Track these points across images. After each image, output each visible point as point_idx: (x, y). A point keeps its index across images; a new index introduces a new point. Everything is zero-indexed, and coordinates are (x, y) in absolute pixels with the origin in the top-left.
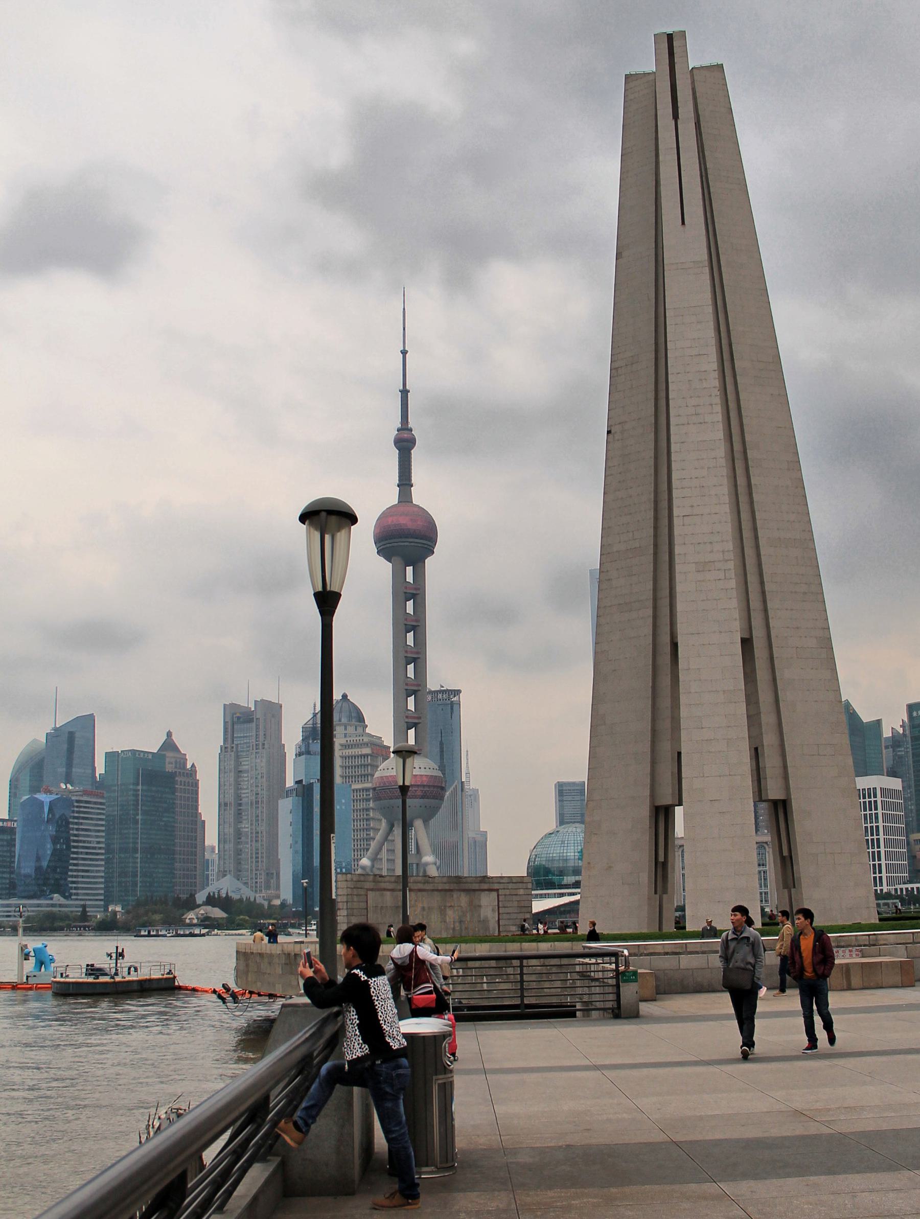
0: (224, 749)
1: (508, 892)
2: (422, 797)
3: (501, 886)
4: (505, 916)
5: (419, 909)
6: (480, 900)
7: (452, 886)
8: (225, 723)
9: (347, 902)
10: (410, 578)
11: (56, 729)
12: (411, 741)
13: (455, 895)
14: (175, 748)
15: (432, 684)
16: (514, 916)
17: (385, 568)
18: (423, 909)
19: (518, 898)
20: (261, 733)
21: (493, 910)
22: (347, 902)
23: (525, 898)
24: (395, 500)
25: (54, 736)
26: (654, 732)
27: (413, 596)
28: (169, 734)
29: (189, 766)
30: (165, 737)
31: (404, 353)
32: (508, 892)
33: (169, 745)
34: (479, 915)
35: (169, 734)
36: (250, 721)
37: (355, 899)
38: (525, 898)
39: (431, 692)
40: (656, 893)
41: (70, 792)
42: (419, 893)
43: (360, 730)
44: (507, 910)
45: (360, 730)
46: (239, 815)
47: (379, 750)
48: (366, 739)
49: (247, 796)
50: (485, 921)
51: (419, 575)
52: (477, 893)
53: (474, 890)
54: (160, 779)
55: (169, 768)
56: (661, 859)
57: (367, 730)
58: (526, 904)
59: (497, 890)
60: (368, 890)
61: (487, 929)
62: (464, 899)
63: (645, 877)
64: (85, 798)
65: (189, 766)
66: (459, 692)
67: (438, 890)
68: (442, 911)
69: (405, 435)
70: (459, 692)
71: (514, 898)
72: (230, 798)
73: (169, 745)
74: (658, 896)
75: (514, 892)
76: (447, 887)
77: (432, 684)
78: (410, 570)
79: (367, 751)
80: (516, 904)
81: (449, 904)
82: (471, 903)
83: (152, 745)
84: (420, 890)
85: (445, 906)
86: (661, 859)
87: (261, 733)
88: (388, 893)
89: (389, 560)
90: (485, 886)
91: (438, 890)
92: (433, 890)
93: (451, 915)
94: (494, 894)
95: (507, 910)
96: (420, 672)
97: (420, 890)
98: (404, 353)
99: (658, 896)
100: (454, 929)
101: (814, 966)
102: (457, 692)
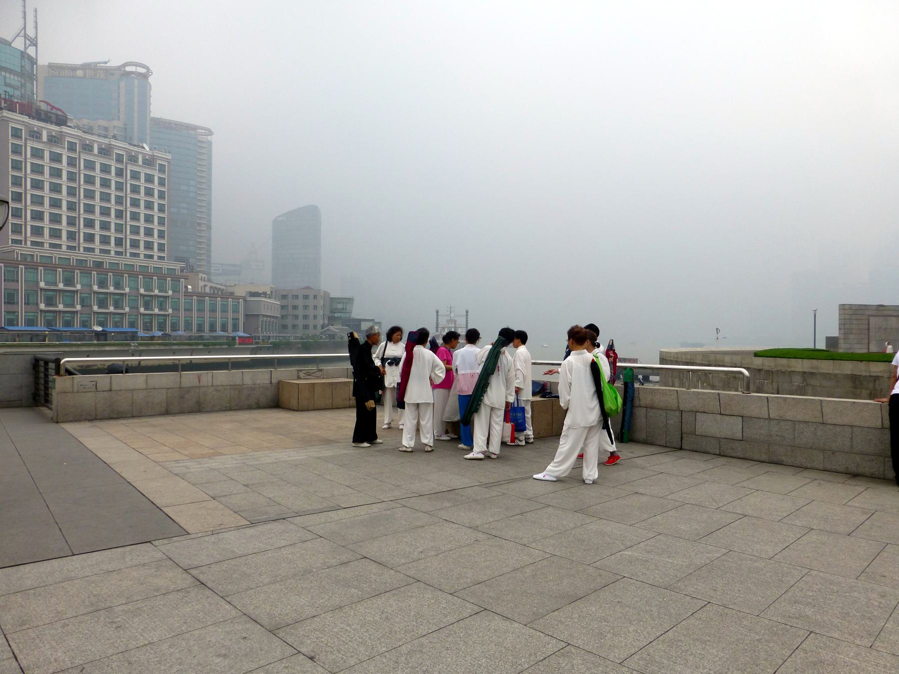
37: (855, 322)
60: (869, 316)
88: (894, 319)
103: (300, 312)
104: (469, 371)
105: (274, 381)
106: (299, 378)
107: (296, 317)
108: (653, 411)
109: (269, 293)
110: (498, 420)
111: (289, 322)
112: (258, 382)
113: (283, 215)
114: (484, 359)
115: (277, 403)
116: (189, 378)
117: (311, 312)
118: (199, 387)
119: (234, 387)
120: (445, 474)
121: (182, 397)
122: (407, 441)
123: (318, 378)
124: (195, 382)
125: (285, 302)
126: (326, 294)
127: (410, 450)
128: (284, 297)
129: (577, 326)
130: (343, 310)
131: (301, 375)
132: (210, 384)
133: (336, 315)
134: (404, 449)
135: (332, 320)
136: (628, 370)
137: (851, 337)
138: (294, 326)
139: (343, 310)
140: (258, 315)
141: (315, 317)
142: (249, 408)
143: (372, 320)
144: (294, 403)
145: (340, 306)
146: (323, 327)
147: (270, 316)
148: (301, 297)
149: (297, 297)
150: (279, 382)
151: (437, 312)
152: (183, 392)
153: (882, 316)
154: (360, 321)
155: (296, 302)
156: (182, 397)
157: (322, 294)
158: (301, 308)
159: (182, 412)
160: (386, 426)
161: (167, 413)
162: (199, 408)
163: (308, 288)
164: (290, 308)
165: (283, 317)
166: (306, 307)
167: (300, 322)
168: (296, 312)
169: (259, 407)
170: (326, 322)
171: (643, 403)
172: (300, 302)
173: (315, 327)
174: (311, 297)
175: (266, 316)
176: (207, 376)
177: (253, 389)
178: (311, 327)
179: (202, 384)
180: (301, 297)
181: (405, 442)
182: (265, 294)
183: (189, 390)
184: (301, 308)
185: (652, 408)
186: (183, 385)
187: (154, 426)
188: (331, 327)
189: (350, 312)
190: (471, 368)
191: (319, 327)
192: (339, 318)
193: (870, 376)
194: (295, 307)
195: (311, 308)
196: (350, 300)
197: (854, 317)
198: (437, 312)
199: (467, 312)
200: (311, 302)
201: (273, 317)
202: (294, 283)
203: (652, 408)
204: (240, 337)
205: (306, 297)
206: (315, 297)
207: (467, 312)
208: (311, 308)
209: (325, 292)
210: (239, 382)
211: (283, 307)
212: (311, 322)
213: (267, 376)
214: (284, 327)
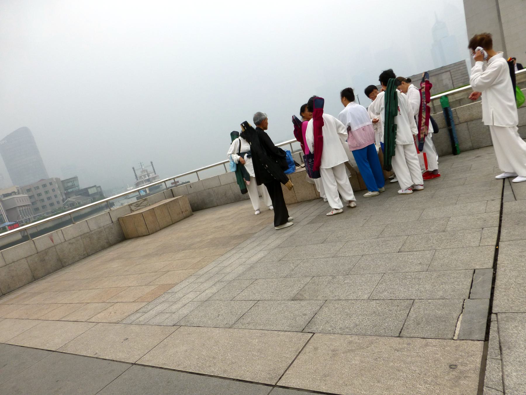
1: (455, 70)
19: (460, 71)
32: (455, 70)
59: (449, 71)
94: (448, 73)
103: (44, 196)
104: (360, 126)
105: (114, 220)
106: (132, 211)
107: (43, 200)
108: (474, 122)
109: (16, 191)
110: (413, 155)
111: (39, 205)
112: (102, 225)
113: (4, 139)
114: (383, 106)
115: (123, 237)
116: (42, 242)
117: (51, 194)
118: (55, 246)
119: (83, 236)
120: (384, 217)
121: (43, 260)
122: (336, 204)
123: (146, 206)
124: (50, 244)
125: (31, 194)
126: (57, 180)
127: (341, 211)
128: (29, 190)
129: (379, 80)
130: (73, 186)
131: (133, 208)
132: (63, 241)
133: (69, 191)
134: (335, 212)
135: (68, 195)
136: (444, 98)
138: (44, 207)
139: (73, 186)
140: (15, 208)
141: (56, 196)
142: (104, 248)
143: (95, 186)
144: (142, 229)
145: (70, 184)
146: (63, 201)
147: (24, 206)
148: (41, 187)
149: (38, 188)
150: (118, 219)
151: (133, 168)
152: (42, 255)
154: (86, 189)
155: (39, 191)
156: (43, 260)
157: (55, 180)
158: (43, 194)
159: (48, 273)
160: (256, 213)
161: (35, 279)
162: (61, 264)
163: (42, 180)
164: (36, 196)
165: (33, 203)
166: (47, 192)
167: (47, 203)
168: (41, 198)
169: (110, 245)
170: (64, 197)
171: (461, 120)
172: (42, 190)
173: (58, 202)
174: (48, 185)
175: (21, 206)
176: (57, 235)
177: (101, 232)
178: (55, 203)
179: (55, 244)
180: (41, 187)
181: (334, 205)
182: (14, 193)
183: (46, 252)
184: (43, 194)
185: (472, 120)
186: (39, 249)
187: (39, 293)
188: (69, 199)
189: (78, 186)
190: (362, 122)
191: (61, 202)
192: (72, 192)
193: (456, 101)
194: (39, 195)
195: (51, 191)
196: (75, 179)
198: (133, 168)
199: (152, 163)
200: (49, 188)
201: (26, 205)
202: (31, 180)
203: (472, 120)
204: (8, 226)
205: (44, 186)
206: (51, 184)
207: (152, 163)
208: (51, 191)
209: (56, 179)
210: (86, 230)
211: (30, 197)
212: (54, 200)
213: (108, 217)
214: (37, 209)
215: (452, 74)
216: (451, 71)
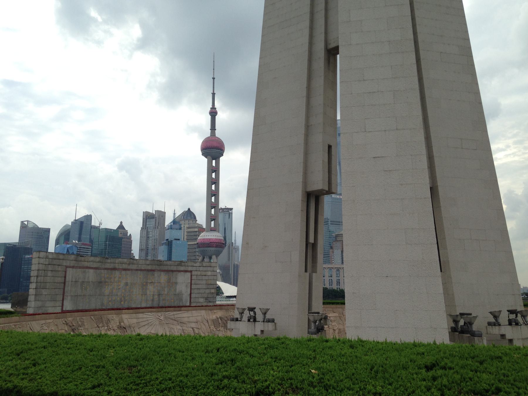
0: (142, 228)
1: (199, 273)
2: (216, 247)
3: (194, 269)
4: (196, 291)
5: (122, 284)
6: (176, 278)
7: (154, 267)
8: (143, 219)
9: (37, 276)
10: (214, 164)
11: (75, 220)
12: (212, 226)
13: (156, 274)
14: (124, 228)
15: (222, 205)
16: (202, 291)
17: (205, 160)
18: (126, 284)
19: (206, 278)
20: (157, 222)
21: (187, 286)
22: (37, 276)
23: (212, 278)
24: (209, 135)
25: (75, 222)
26: (308, 127)
27: (215, 171)
28: (121, 223)
29: (128, 235)
30: (119, 224)
31: (214, 79)
32: (199, 273)
33: (121, 227)
34: (175, 290)
35: (121, 223)
36: (153, 218)
37: (50, 274)
38: (212, 278)
39: (221, 209)
40: (306, 271)
41: (77, 244)
42: (123, 272)
43: (194, 222)
44: (198, 286)
45: (194, 222)
46: (147, 254)
47: (201, 230)
48: (196, 226)
49: (150, 246)
50: (179, 295)
51: (218, 164)
52: (175, 273)
53: (172, 271)
54: (117, 239)
55: (120, 235)
56: (311, 240)
57: (197, 222)
58: (212, 282)
59: (191, 271)
60: (67, 267)
61: (181, 300)
62: (163, 278)
63: (297, 255)
64: (83, 246)
65: (128, 235)
66: (232, 209)
67: (141, 270)
68: (144, 286)
69: (214, 110)
70: (232, 209)
71: (204, 278)
72: (144, 247)
73: (121, 227)
74: (307, 274)
75: (204, 273)
76: (149, 268)
77: (222, 205)
78: (214, 161)
79: (196, 230)
80: (204, 282)
81: (149, 281)
82: (169, 281)
83: (114, 226)
84: (125, 270)
85: (147, 283)
86: (311, 240)
87: (157, 222)
88: (91, 271)
89: (206, 157)
90: (182, 268)
91: (141, 270)
92: (137, 270)
93: (151, 290)
94: (189, 274)
95: (198, 286)
96: (217, 200)
97: (125, 270)
98: (214, 79)
99: (307, 274)
100: (153, 300)
101: (57, 242)
102: (231, 209)
137: (44, 292)
153: (80, 268)
197: (50, 268)
215: (194, 277)
216: (193, 273)
